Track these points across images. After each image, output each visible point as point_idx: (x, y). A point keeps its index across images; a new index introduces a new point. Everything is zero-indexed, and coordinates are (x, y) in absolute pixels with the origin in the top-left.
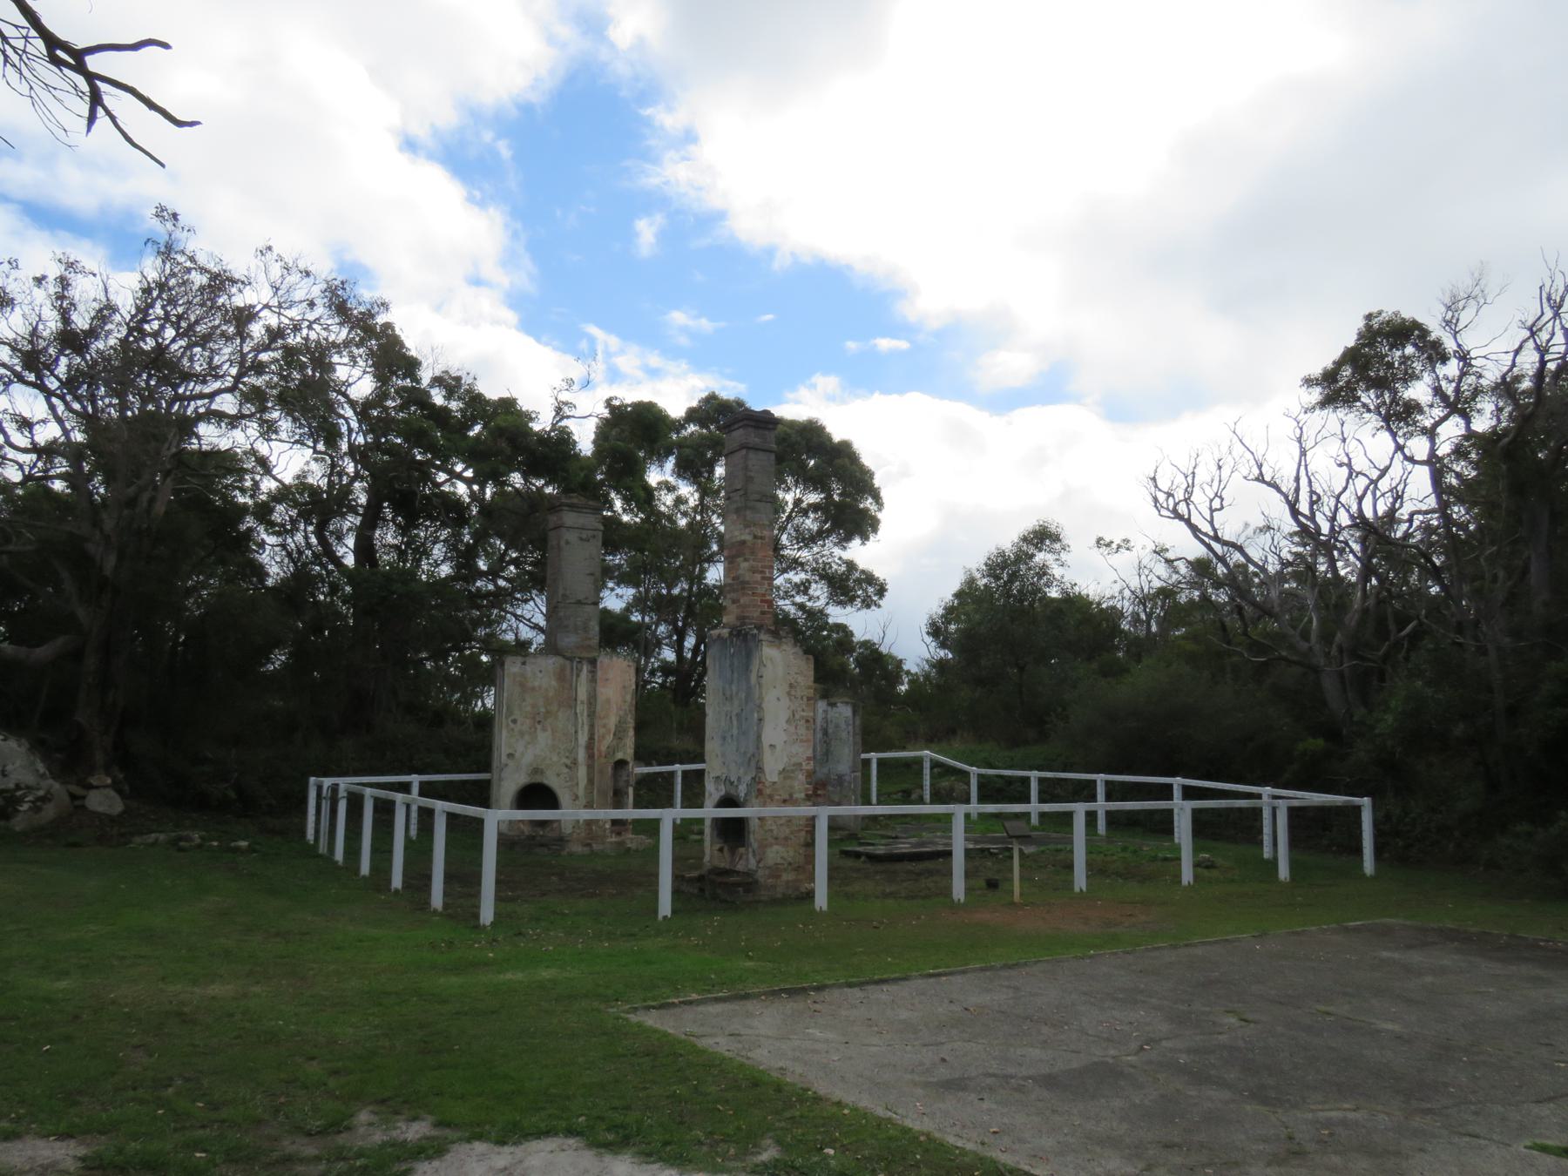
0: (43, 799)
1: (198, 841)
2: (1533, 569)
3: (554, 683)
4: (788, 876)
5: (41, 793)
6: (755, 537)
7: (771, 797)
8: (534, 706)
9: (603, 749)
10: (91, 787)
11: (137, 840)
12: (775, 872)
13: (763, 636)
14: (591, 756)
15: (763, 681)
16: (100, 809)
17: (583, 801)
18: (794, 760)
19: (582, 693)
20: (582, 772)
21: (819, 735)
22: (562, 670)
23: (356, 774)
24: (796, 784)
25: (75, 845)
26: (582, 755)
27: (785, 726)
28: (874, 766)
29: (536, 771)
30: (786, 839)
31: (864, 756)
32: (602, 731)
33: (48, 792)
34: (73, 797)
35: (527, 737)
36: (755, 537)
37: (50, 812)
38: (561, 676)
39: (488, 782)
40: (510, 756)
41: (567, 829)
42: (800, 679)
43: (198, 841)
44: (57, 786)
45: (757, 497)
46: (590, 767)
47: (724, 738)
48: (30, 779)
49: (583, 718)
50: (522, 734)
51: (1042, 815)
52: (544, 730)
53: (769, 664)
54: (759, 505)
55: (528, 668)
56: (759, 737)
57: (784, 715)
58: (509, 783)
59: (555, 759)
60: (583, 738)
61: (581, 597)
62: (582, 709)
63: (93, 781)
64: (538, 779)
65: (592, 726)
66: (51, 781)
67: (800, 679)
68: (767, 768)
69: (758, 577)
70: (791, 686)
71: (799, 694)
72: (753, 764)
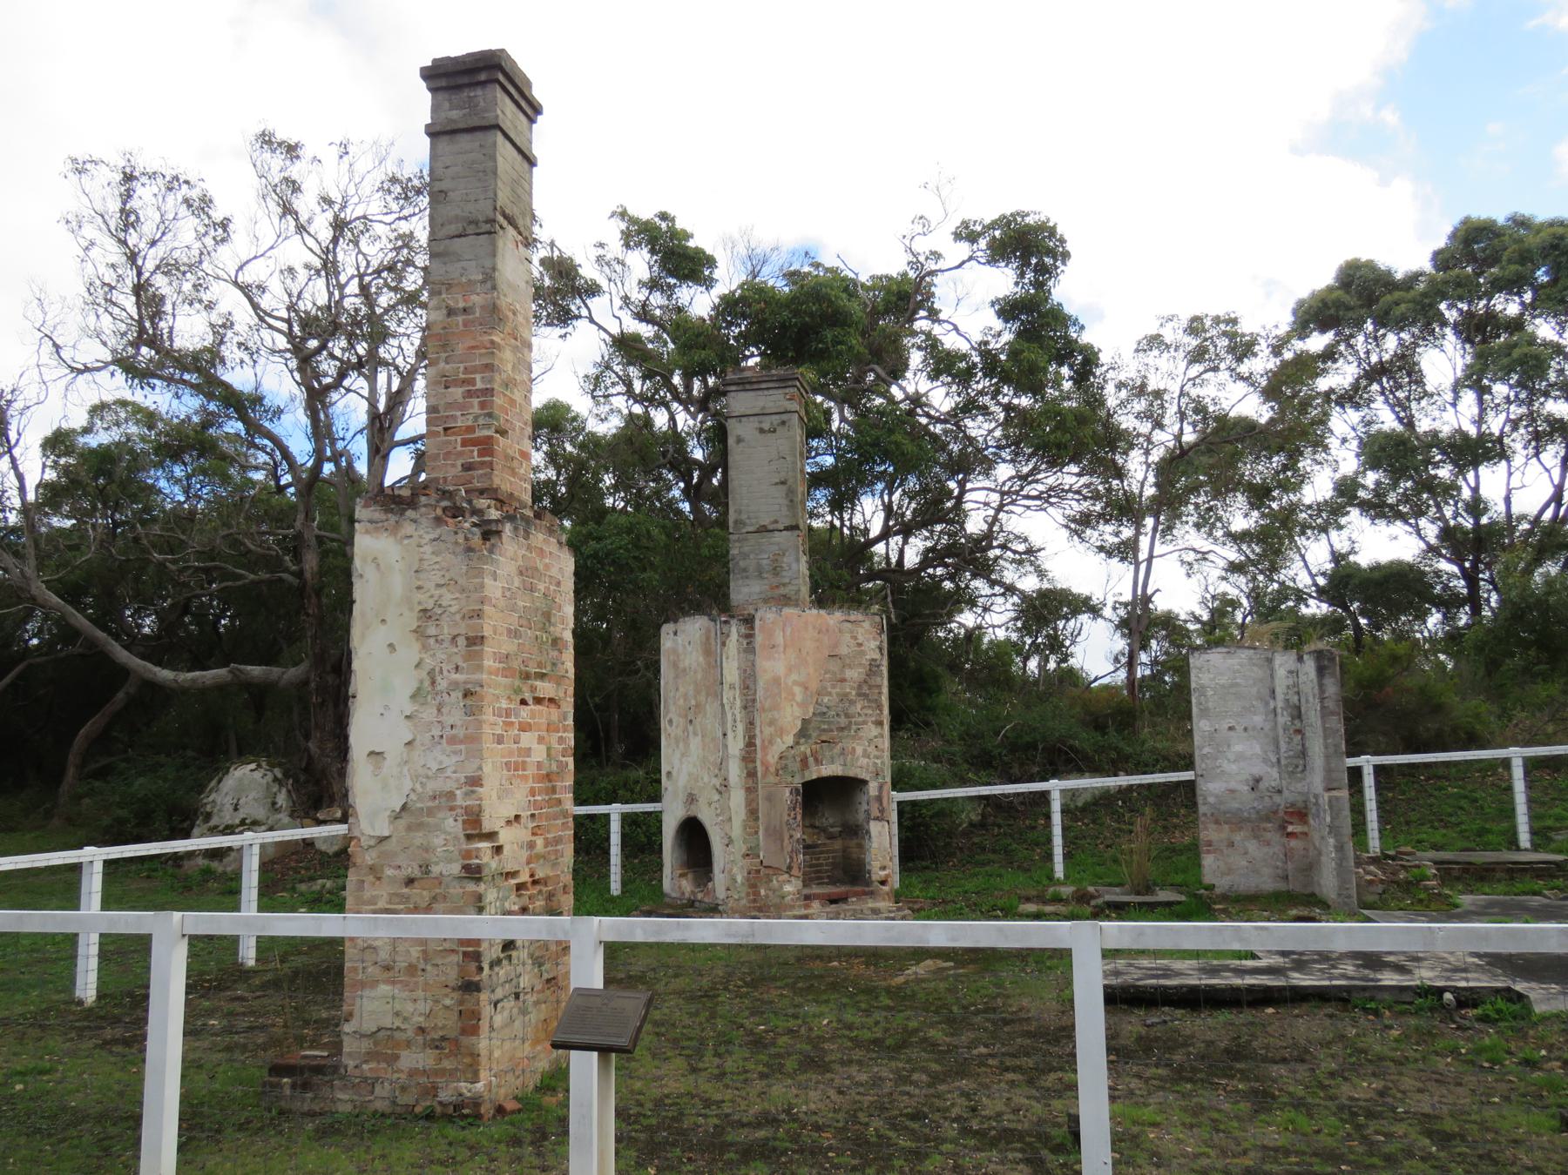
4: (415, 1059)
6: (451, 312)
9: (772, 759)
12: (385, 1044)
14: (752, 774)
18: (432, 786)
19: (731, 673)
20: (737, 798)
21: (1284, 719)
24: (438, 841)
26: (735, 771)
28: (1369, 780)
30: (412, 969)
31: (1351, 762)
32: (768, 731)
36: (451, 312)
40: (669, 773)
42: (447, 597)
46: (750, 791)
49: (735, 712)
55: (679, 639)
57: (404, 683)
60: (736, 745)
61: (765, 521)
62: (732, 698)
67: (447, 597)
69: (457, 393)
70: (425, 614)
71: (447, 631)
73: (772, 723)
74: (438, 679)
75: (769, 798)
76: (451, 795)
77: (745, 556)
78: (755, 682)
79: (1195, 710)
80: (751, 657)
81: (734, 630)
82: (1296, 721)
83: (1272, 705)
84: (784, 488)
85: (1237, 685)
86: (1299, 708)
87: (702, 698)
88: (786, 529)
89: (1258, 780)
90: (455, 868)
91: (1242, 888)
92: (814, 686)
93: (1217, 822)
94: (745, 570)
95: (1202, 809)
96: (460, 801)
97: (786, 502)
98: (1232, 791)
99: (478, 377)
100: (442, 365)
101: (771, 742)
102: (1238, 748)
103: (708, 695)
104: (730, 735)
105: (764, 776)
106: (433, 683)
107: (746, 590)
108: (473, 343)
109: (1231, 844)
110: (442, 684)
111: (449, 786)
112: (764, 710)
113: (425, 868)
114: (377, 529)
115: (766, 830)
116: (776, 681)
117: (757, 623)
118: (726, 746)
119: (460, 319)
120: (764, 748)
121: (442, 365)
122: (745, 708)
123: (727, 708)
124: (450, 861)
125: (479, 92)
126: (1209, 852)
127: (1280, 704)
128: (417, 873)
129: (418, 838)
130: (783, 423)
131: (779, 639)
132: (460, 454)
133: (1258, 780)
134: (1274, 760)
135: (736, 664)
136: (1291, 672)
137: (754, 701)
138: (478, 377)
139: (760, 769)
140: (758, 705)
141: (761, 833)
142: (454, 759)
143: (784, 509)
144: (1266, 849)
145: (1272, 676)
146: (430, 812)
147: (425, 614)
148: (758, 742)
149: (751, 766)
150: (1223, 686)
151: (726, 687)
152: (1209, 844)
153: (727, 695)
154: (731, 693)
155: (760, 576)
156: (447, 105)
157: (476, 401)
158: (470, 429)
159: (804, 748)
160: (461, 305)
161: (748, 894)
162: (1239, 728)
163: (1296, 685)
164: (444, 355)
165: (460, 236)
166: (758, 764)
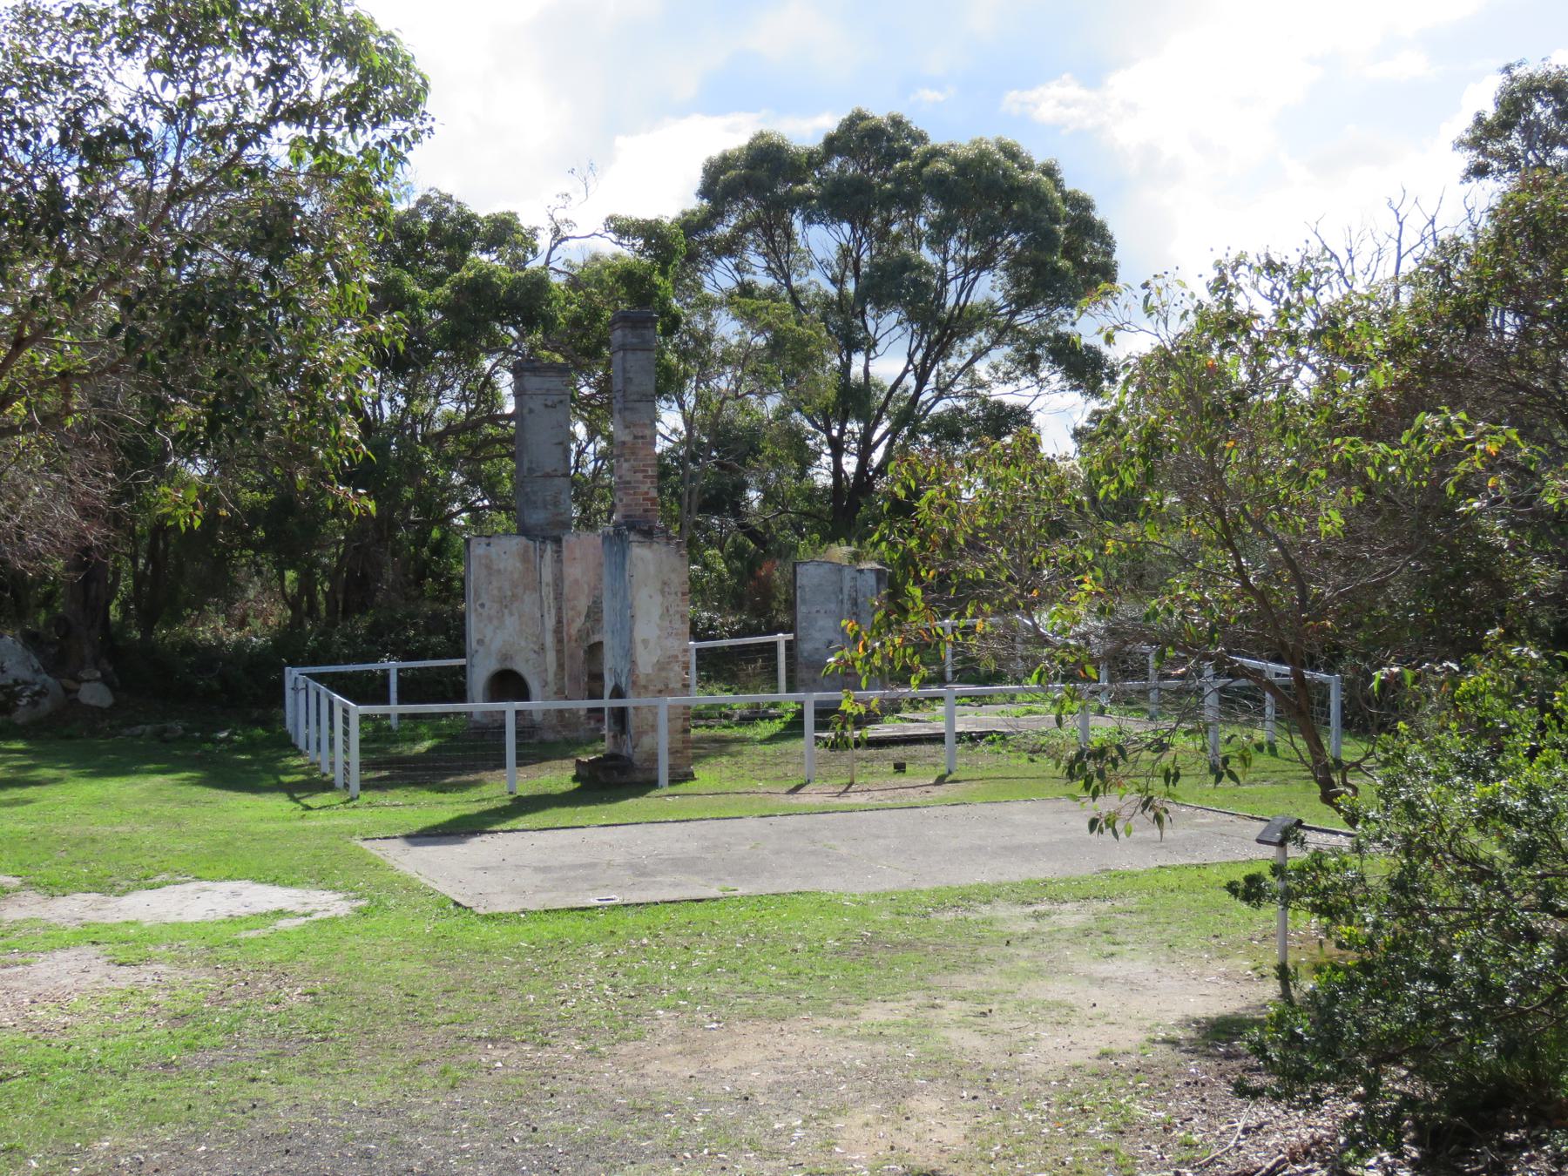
0: (39, 694)
1: (181, 732)
2: (605, 606)
5: (37, 688)
6: (636, 437)
7: (645, 687)
8: (500, 589)
9: (573, 632)
10: (80, 681)
11: (126, 731)
13: (632, 537)
14: (560, 641)
16: (93, 702)
17: (552, 687)
20: (551, 657)
22: (526, 550)
23: (304, 665)
25: (69, 737)
26: (549, 640)
29: (505, 657)
33: (43, 686)
34: (67, 691)
35: (495, 622)
36: (636, 437)
37: (46, 705)
38: (525, 558)
39: (463, 668)
41: (538, 718)
42: (673, 576)
43: (181, 732)
44: (51, 680)
46: (559, 652)
48: (26, 674)
50: (490, 619)
51: (401, 716)
52: (511, 614)
54: (637, 405)
55: (493, 549)
57: (656, 612)
58: (480, 672)
59: (523, 644)
60: (550, 622)
61: (549, 470)
62: (548, 592)
63: (84, 675)
64: (509, 665)
65: (559, 609)
66: (45, 676)
68: (640, 661)
69: (640, 476)
70: (665, 583)
73: (573, 609)
95: (800, 659)
96: (681, 658)
116: (576, 582)
129: (664, 674)
131: (578, 554)
147: (665, 583)
153: (545, 590)
155: (545, 507)
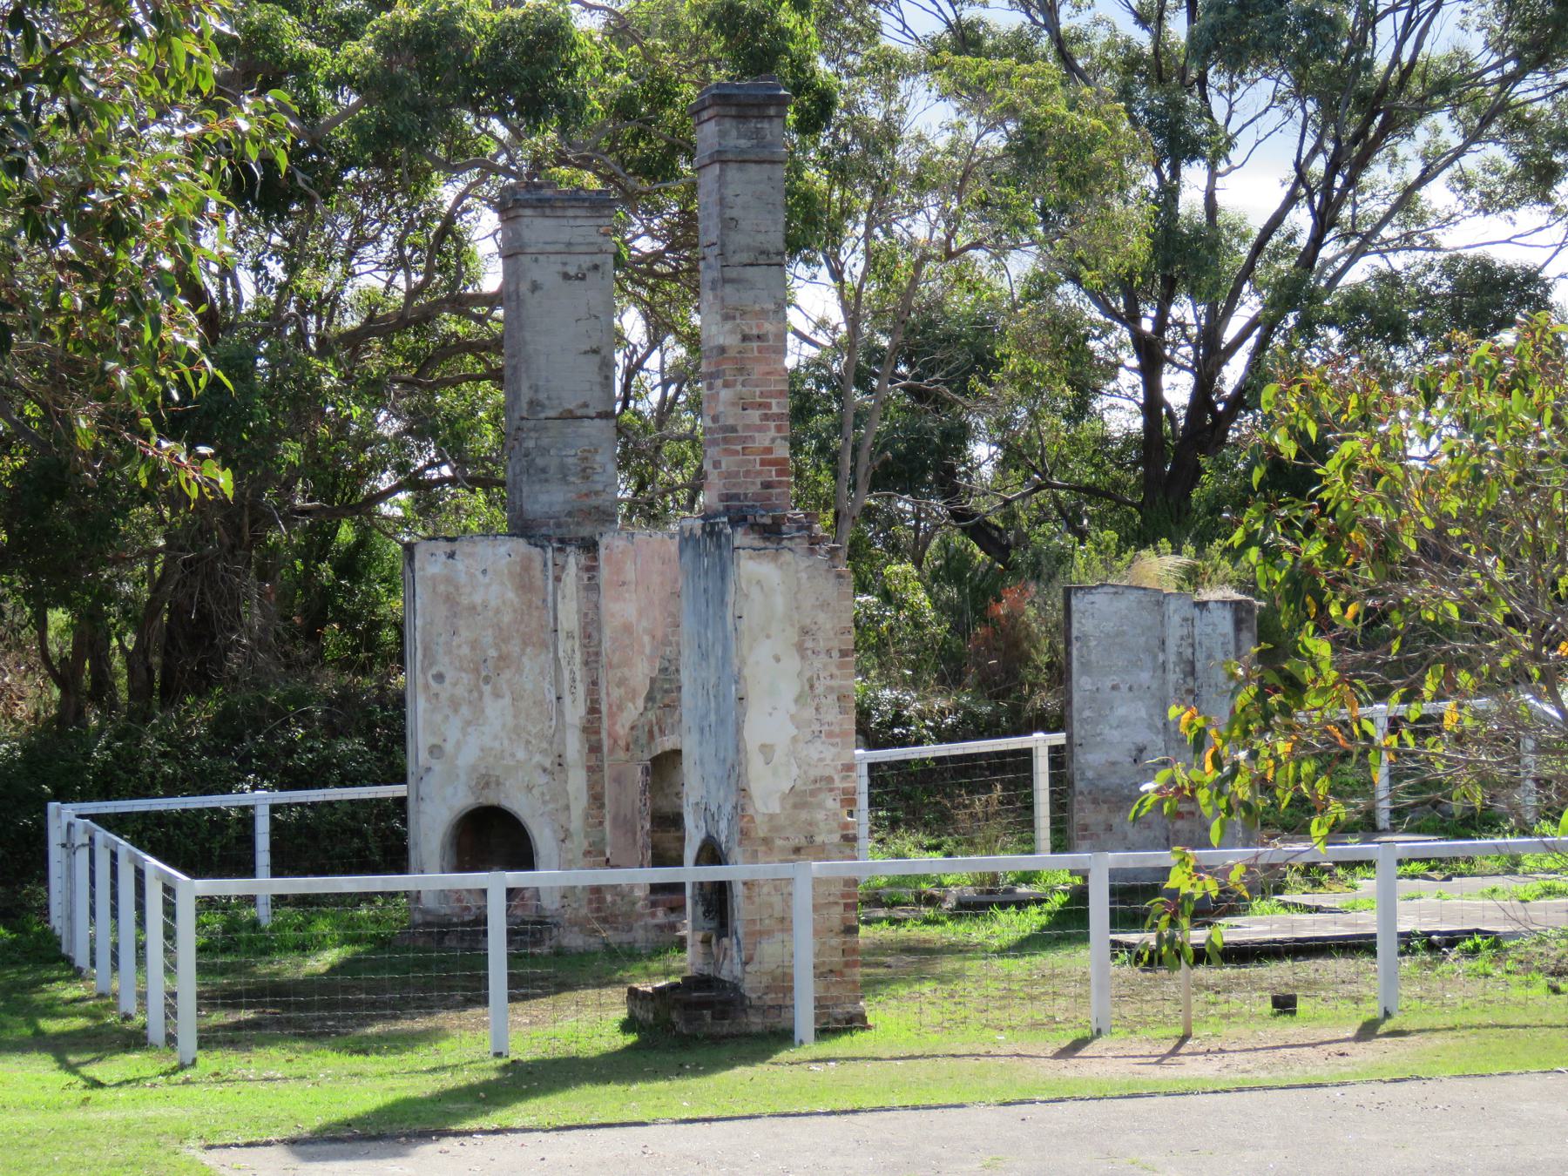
3: (511, 595)
6: (745, 338)
9: (622, 730)
14: (595, 749)
15: (743, 626)
17: (579, 843)
18: (814, 773)
20: (577, 781)
21: (1174, 676)
22: (526, 567)
24: (820, 816)
26: (574, 747)
27: (793, 709)
29: (486, 781)
32: (616, 693)
35: (465, 710)
36: (745, 338)
40: (435, 751)
41: (550, 903)
42: (822, 617)
45: (745, 257)
46: (593, 770)
47: (702, 730)
49: (574, 668)
50: (455, 705)
51: (279, 900)
52: (497, 695)
53: (755, 593)
55: (460, 564)
56: (739, 729)
57: (789, 688)
59: (521, 755)
60: (575, 712)
64: (490, 798)
69: (754, 416)
70: (805, 632)
72: (733, 780)
73: (622, 682)
74: (817, 684)
75: (618, 780)
76: (830, 779)
77: (544, 451)
78: (599, 630)
79: (1075, 665)
80: (594, 597)
81: (572, 560)
82: (1190, 680)
83: (1161, 658)
84: (597, 359)
85: (1124, 633)
86: (1192, 664)
87: (514, 648)
88: (600, 416)
89: (1141, 750)
90: (836, 838)
91: (273, 1052)
92: (659, 634)
93: (1095, 801)
94: (544, 470)
95: (1079, 785)
96: (838, 784)
97: (599, 379)
98: (1113, 764)
99: (774, 401)
100: (739, 387)
101: (621, 708)
102: (1121, 711)
103: (525, 644)
104: (567, 699)
105: (611, 751)
106: (812, 687)
107: (544, 498)
108: (767, 369)
109: (1109, 828)
110: (820, 689)
111: (828, 772)
112: (611, 666)
113: (810, 839)
114: (759, 556)
115: (615, 819)
116: (627, 629)
117: (602, 551)
118: (561, 713)
119: (755, 345)
120: (612, 715)
121: (739, 387)
122: (586, 663)
123: (563, 663)
124: (831, 832)
125: (766, 125)
126: (1084, 838)
127: (1172, 658)
128: (803, 842)
129: (804, 815)
130: (596, 267)
131: (630, 574)
132: (759, 473)
133: (1141, 750)
134: (1160, 725)
135: (573, 606)
136: (1185, 620)
137: (597, 654)
138: (774, 401)
139: (606, 743)
140: (604, 659)
141: (607, 824)
142: (833, 750)
143: (597, 388)
144: (1147, 832)
145: (1162, 624)
146: (813, 793)
148: (604, 708)
149: (593, 738)
150: (1108, 635)
151: (562, 635)
152: (1085, 828)
153: (564, 646)
154: (569, 643)
155: (564, 479)
156: (734, 133)
157: (772, 424)
158: (769, 450)
159: (651, 715)
160: (755, 332)
161: (590, 901)
162: (1124, 688)
163: (1191, 635)
164: (741, 379)
165: (752, 265)
166: (604, 735)
